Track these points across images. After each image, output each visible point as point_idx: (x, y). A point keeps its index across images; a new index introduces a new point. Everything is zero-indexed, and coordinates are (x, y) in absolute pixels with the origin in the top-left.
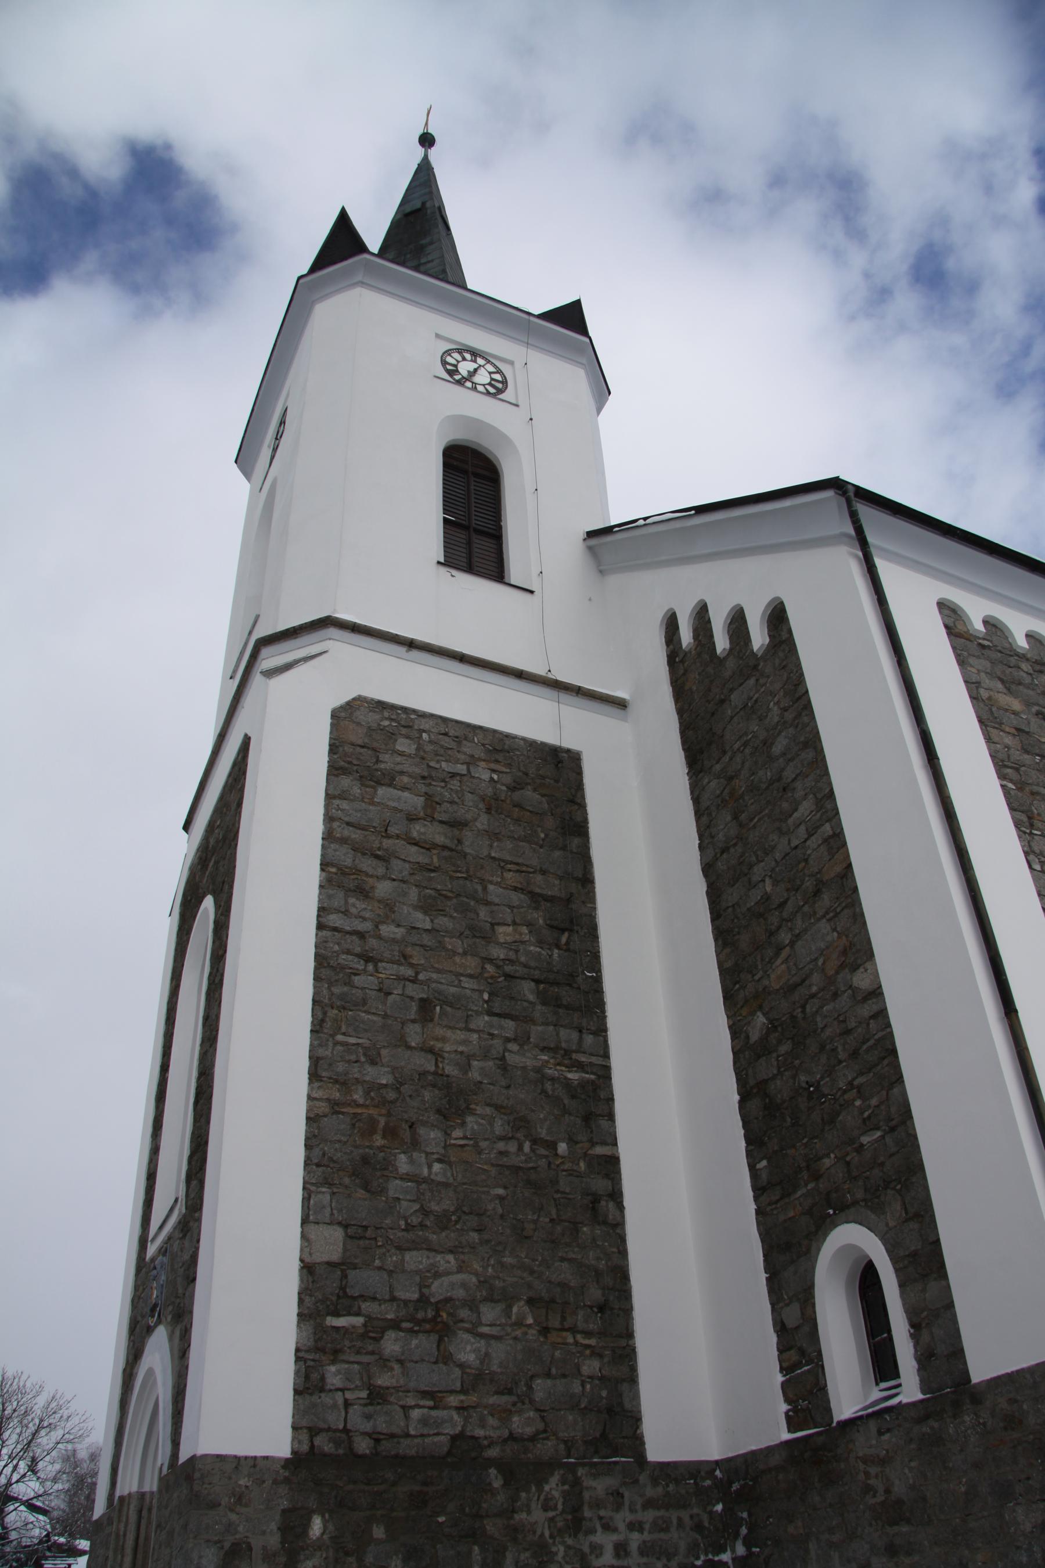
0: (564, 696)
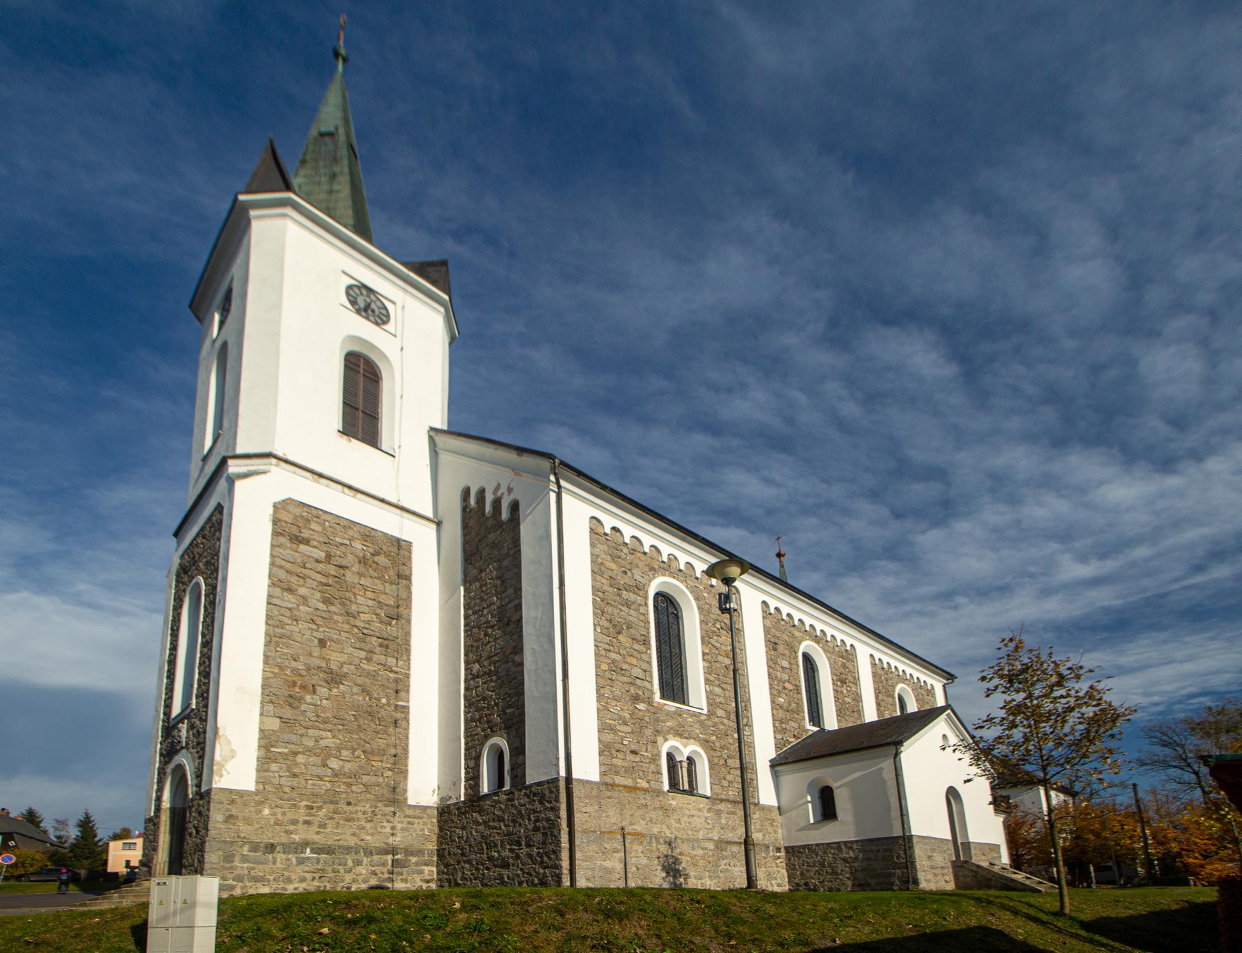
0: (405, 514)
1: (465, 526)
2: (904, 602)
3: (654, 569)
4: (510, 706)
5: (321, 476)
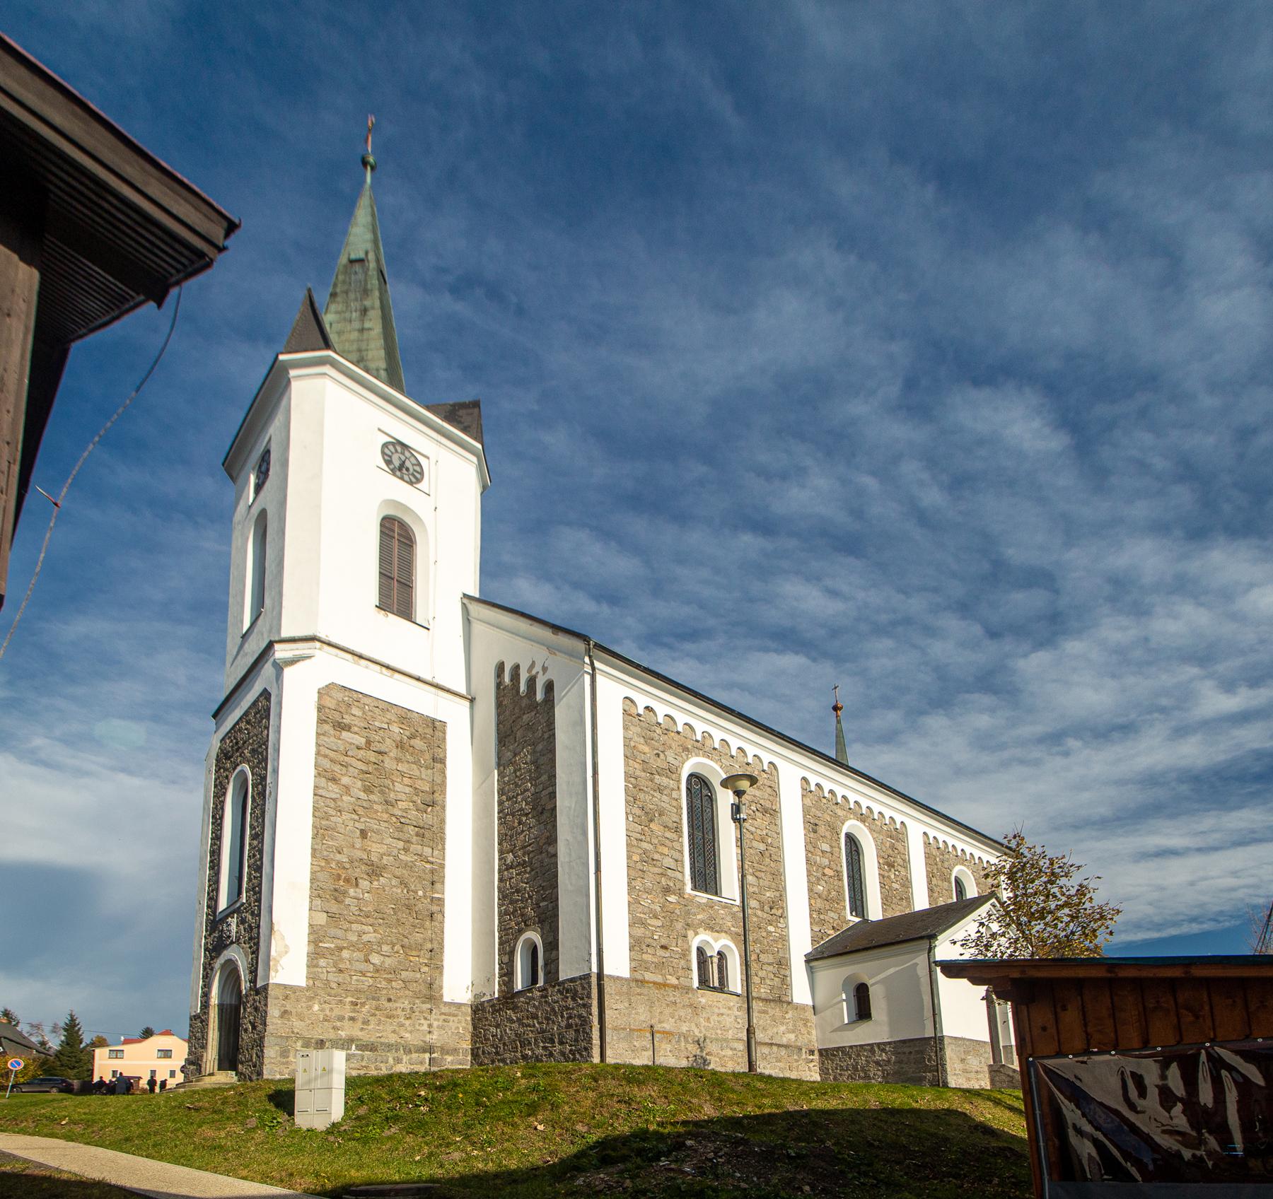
1: (499, 705)
2: (1002, 747)
3: (687, 749)
4: (544, 899)
5: (361, 657)
